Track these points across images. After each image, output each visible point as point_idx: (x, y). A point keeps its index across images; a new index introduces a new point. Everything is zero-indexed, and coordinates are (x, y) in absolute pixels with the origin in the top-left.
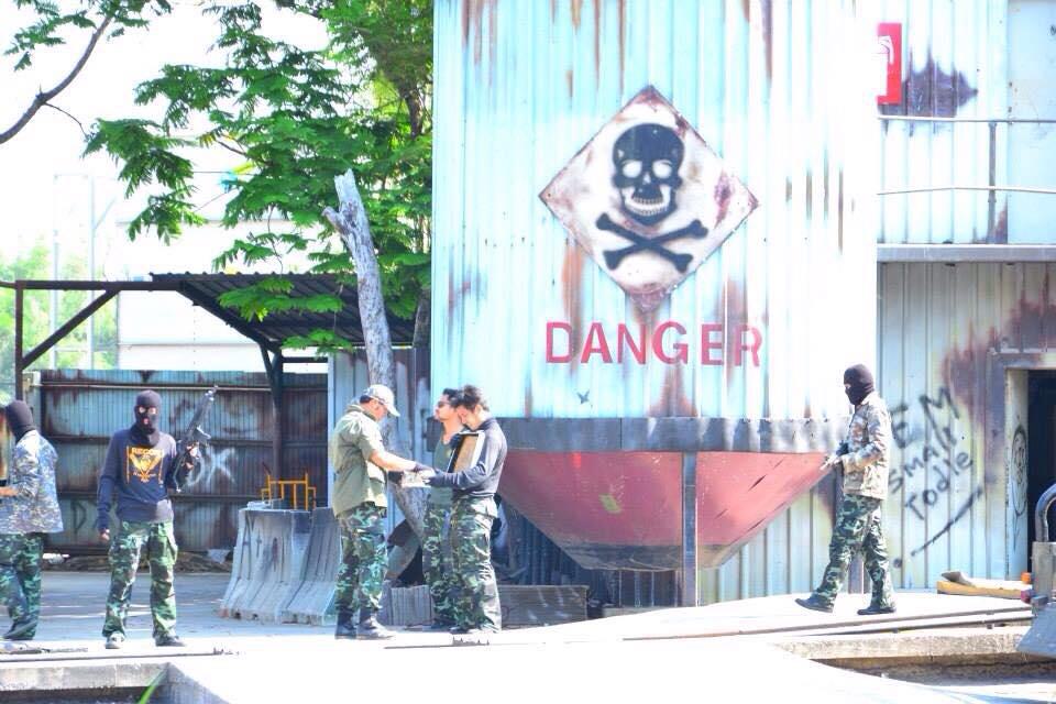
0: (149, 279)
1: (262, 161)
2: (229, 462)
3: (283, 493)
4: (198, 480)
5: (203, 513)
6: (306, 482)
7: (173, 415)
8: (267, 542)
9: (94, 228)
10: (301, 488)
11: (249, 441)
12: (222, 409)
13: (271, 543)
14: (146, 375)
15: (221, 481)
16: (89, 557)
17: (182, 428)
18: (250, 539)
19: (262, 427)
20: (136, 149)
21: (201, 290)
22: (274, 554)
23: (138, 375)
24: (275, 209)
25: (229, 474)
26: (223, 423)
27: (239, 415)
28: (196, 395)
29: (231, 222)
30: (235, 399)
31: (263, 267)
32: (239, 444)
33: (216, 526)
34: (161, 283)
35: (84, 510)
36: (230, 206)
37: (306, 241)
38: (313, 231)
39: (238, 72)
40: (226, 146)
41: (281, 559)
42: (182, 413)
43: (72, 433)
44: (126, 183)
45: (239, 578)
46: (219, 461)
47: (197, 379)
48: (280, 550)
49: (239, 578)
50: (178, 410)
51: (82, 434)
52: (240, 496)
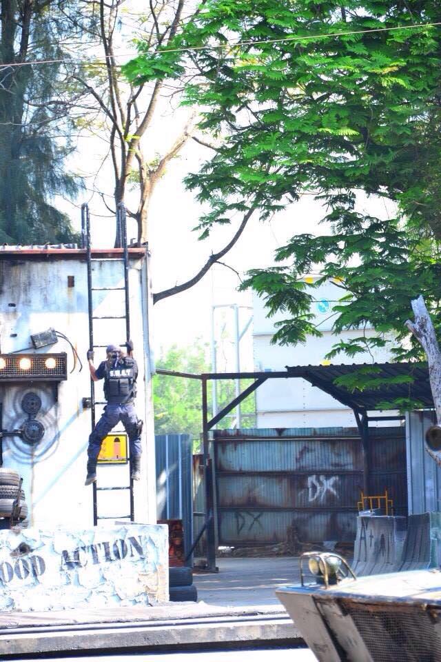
0: (286, 370)
1: (358, 292)
2: (335, 485)
3: (371, 504)
4: (315, 497)
5: (319, 518)
6: (386, 497)
7: (298, 456)
8: (377, 536)
9: (239, 338)
10: (383, 501)
11: (347, 472)
12: (330, 451)
13: (380, 537)
14: (280, 431)
15: (330, 497)
16: (247, 548)
17: (304, 464)
18: (365, 535)
19: (356, 463)
20: (280, 290)
21: (319, 376)
22: (382, 546)
23: (275, 431)
24: (368, 322)
25: (335, 493)
26: (330, 460)
27: (340, 455)
28: (313, 443)
29: (338, 331)
30: (338, 445)
31: (359, 359)
32: (341, 473)
33: (327, 526)
34: (293, 372)
35: (243, 518)
36: (337, 322)
37: (385, 342)
38: (390, 335)
39: (340, 237)
40: (336, 285)
41: (387, 548)
42: (304, 455)
43: (235, 469)
44: (269, 309)
45: (359, 561)
46: (328, 484)
47: (312, 432)
48: (192, 521)
49: (359, 561)
50: (301, 453)
51: (241, 470)
52: (343, 507)
